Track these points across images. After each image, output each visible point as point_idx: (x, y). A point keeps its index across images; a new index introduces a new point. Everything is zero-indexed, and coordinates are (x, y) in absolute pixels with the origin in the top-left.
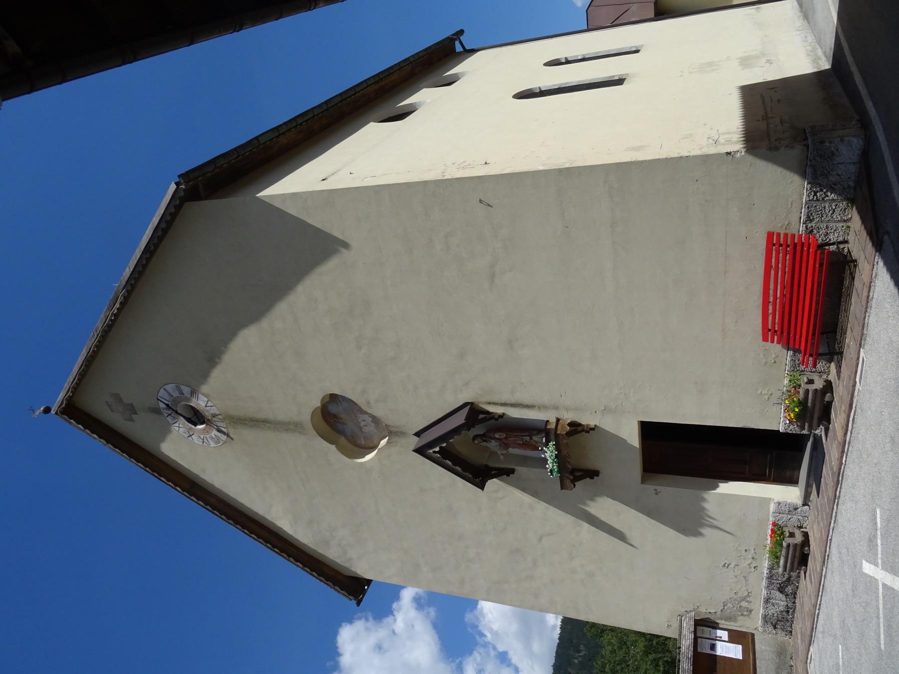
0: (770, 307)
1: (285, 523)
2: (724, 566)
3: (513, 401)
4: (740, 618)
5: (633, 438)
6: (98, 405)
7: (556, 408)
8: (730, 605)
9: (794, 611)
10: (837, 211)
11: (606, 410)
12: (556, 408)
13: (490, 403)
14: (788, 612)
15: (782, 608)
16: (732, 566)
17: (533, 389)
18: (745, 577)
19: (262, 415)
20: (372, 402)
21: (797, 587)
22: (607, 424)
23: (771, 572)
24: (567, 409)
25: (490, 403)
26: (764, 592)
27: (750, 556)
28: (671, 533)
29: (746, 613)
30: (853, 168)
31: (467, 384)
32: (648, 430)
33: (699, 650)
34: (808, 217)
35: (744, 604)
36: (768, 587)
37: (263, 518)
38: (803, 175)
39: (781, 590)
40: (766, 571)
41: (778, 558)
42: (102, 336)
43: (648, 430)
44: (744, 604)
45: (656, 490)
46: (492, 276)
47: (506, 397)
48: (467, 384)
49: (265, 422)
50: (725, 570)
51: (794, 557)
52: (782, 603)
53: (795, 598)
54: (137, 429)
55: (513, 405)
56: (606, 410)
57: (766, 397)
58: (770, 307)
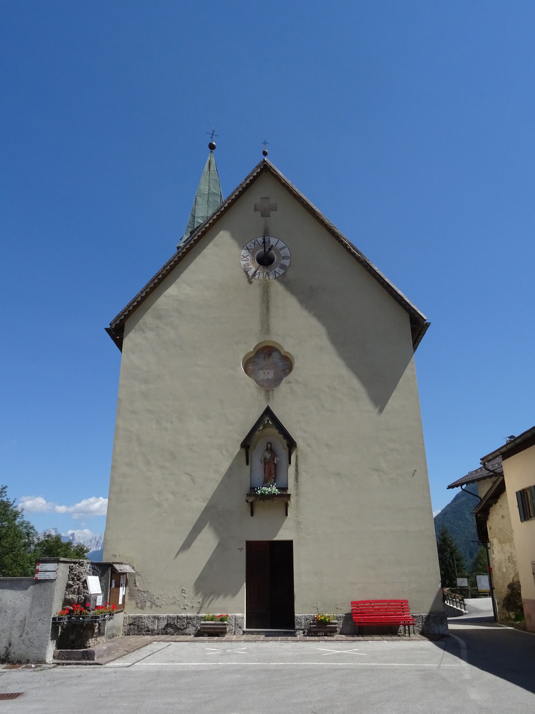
0: (368, 604)
1: (173, 292)
2: (183, 590)
3: (299, 470)
4: (134, 602)
5: (282, 536)
6: (265, 190)
7: (297, 495)
8: (146, 595)
9: (149, 635)
10: (418, 628)
11: (298, 523)
12: (297, 495)
13: (297, 457)
14: (148, 631)
15: (150, 627)
16: (183, 595)
17: (310, 482)
18: (175, 603)
19: (272, 309)
20: (290, 385)
21: (172, 635)
22: (289, 522)
23: (184, 618)
24: (297, 501)
25: (297, 457)
26: (164, 615)
27: (194, 605)
28: (207, 557)
29: (139, 605)
30: (437, 632)
31: (309, 446)
32: (288, 546)
33: (121, 576)
34: (415, 616)
35: (148, 604)
36: (168, 618)
37: (178, 276)
38: (431, 613)
39: (168, 625)
40: (184, 615)
41: (212, 620)
42: (330, 229)
43: (288, 546)
44: (148, 604)
45: (242, 549)
46: (377, 470)
47: (301, 466)
48: (309, 446)
49: (268, 309)
50: (179, 591)
51: (215, 629)
52: (156, 627)
53: (163, 634)
54: (246, 212)
55: (297, 470)
56: (298, 523)
57: (316, 606)
58: (368, 604)
